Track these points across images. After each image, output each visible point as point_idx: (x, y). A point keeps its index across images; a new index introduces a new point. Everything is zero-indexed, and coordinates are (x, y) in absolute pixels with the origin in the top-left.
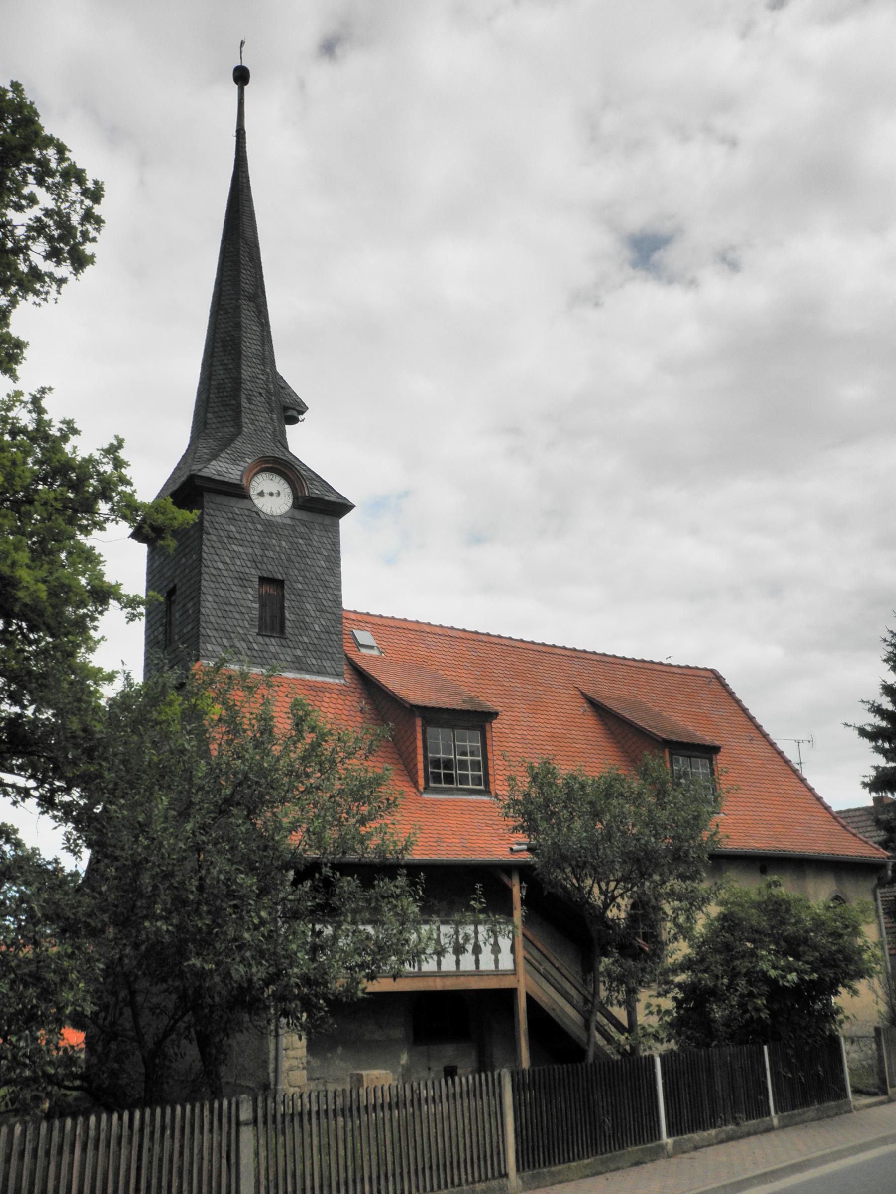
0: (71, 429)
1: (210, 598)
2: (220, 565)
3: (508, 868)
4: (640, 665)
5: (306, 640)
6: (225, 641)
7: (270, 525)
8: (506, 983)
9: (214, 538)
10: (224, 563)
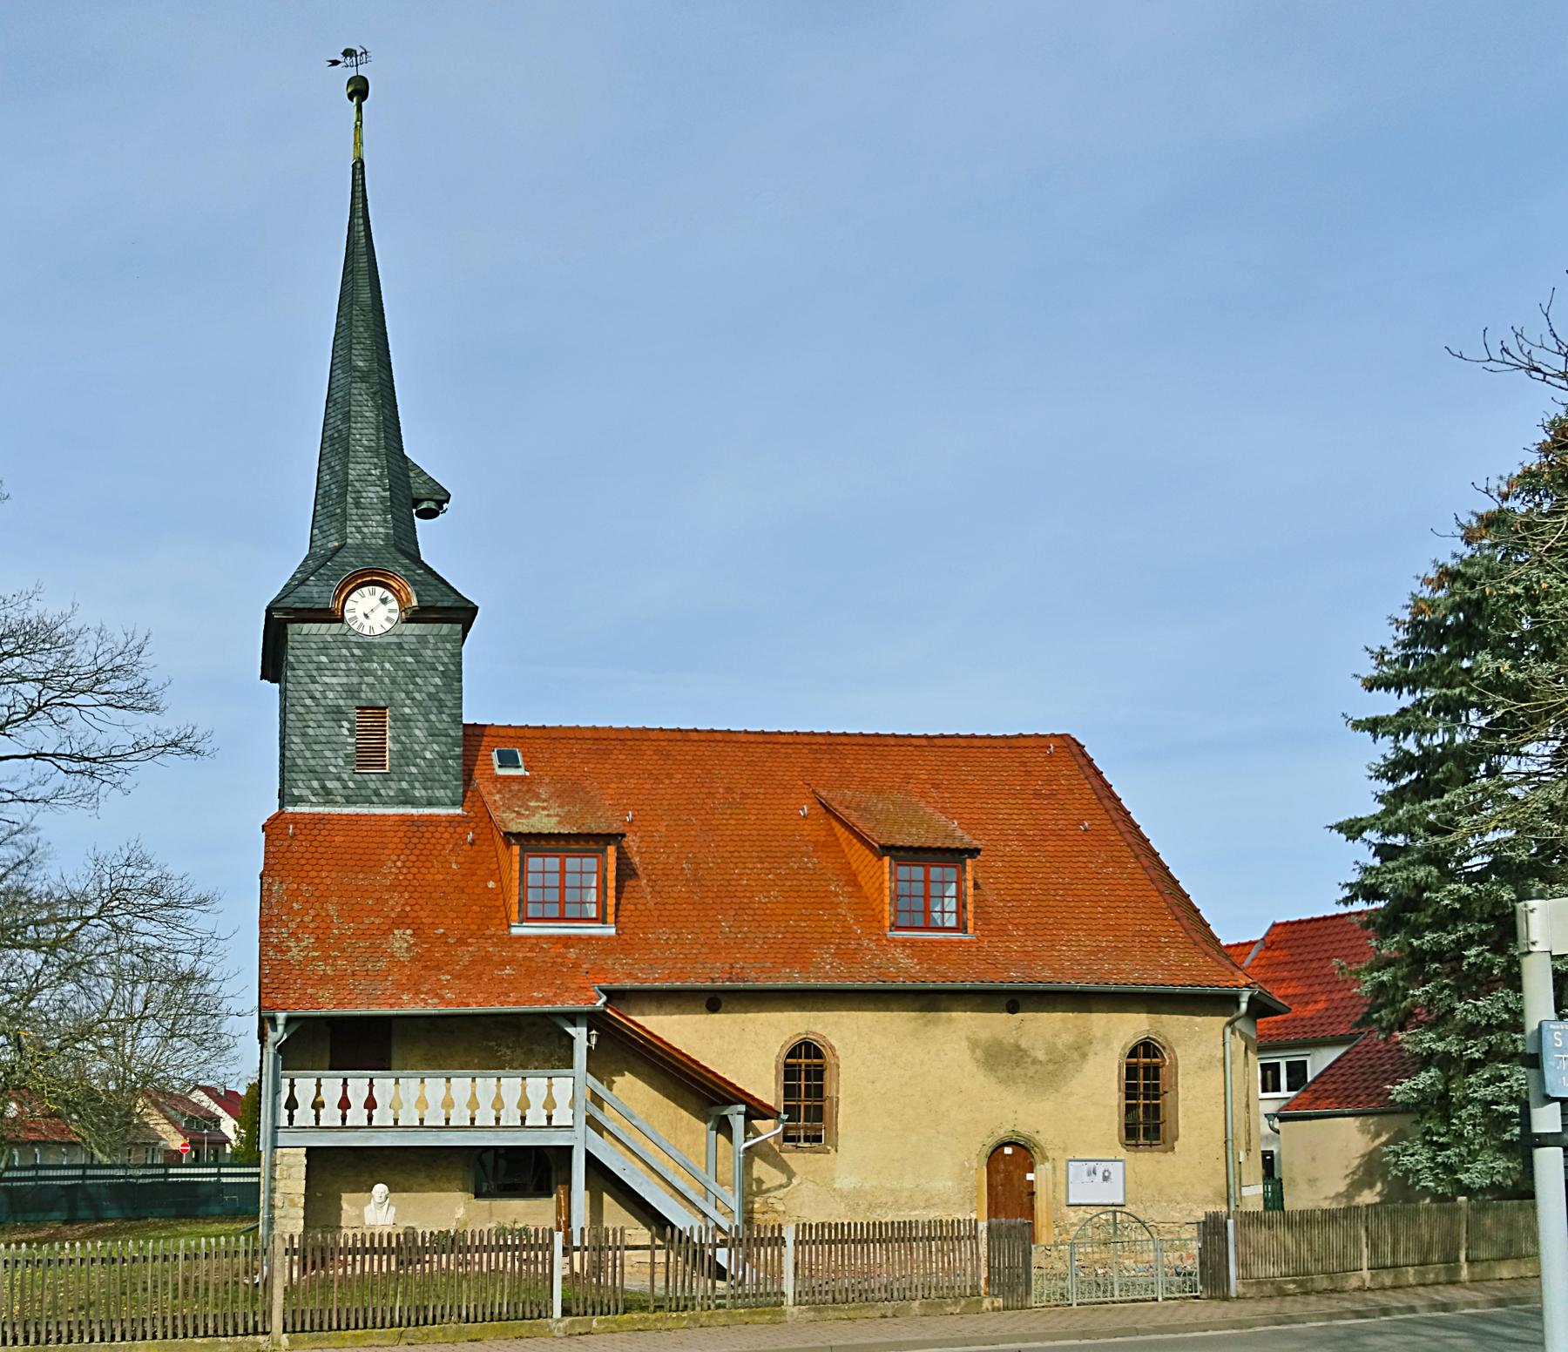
0: (1385, 757)
1: (296, 740)
2: (308, 702)
3: (573, 1018)
4: (760, 739)
5: (414, 770)
6: (315, 784)
7: (369, 648)
8: (559, 1140)
9: (301, 673)
10: (313, 697)
